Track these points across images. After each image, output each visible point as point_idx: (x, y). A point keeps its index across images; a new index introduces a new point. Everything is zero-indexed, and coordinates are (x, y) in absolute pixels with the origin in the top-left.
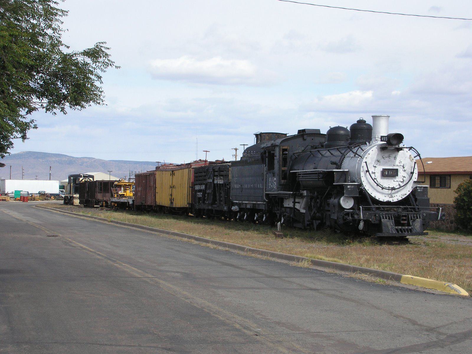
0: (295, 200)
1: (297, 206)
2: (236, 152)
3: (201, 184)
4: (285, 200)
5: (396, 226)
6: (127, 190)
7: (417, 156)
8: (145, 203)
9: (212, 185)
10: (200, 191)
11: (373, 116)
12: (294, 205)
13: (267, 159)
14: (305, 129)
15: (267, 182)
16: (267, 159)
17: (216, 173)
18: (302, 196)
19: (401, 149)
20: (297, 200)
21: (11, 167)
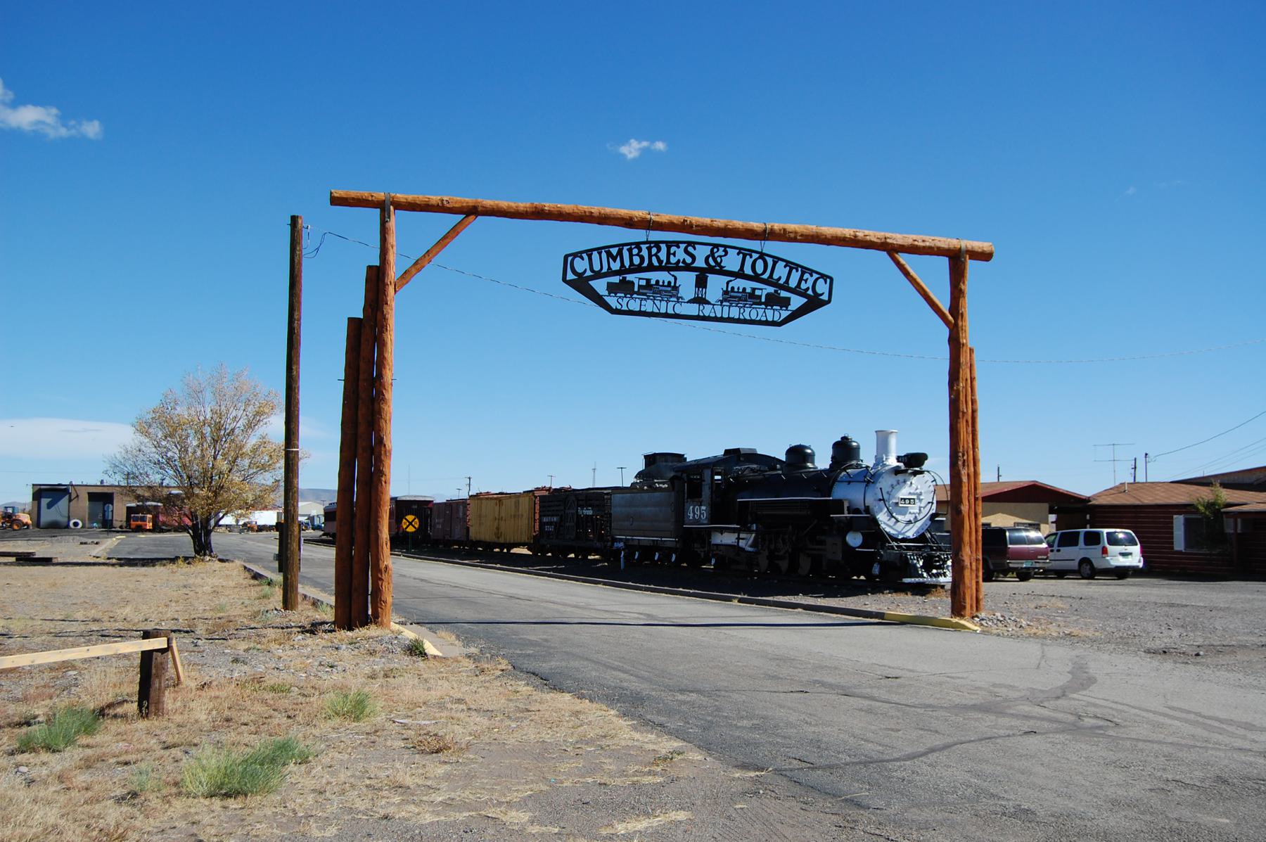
0: (739, 536)
1: (742, 543)
2: (1114, 468)
3: (553, 516)
4: (712, 534)
5: (298, 451)
6: (125, 836)
7: (1135, 480)
8: (450, 537)
9: (575, 517)
10: (550, 523)
11: (876, 432)
12: (738, 542)
13: (686, 484)
14: (739, 449)
15: (1171, 586)
16: (686, 484)
17: (581, 503)
18: (749, 531)
19: (921, 472)
20: (742, 536)
21: (470, 478)
